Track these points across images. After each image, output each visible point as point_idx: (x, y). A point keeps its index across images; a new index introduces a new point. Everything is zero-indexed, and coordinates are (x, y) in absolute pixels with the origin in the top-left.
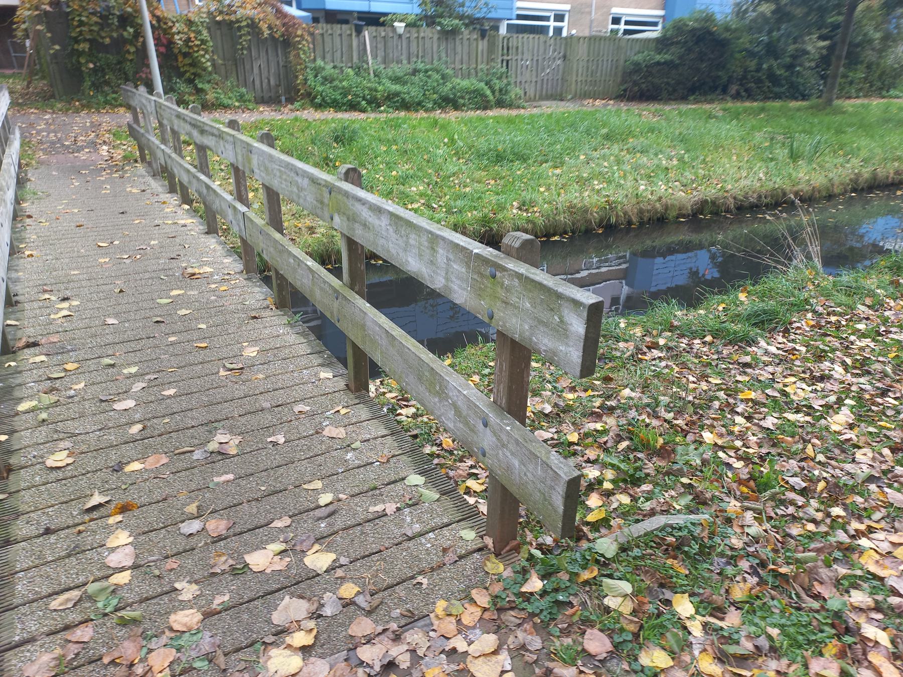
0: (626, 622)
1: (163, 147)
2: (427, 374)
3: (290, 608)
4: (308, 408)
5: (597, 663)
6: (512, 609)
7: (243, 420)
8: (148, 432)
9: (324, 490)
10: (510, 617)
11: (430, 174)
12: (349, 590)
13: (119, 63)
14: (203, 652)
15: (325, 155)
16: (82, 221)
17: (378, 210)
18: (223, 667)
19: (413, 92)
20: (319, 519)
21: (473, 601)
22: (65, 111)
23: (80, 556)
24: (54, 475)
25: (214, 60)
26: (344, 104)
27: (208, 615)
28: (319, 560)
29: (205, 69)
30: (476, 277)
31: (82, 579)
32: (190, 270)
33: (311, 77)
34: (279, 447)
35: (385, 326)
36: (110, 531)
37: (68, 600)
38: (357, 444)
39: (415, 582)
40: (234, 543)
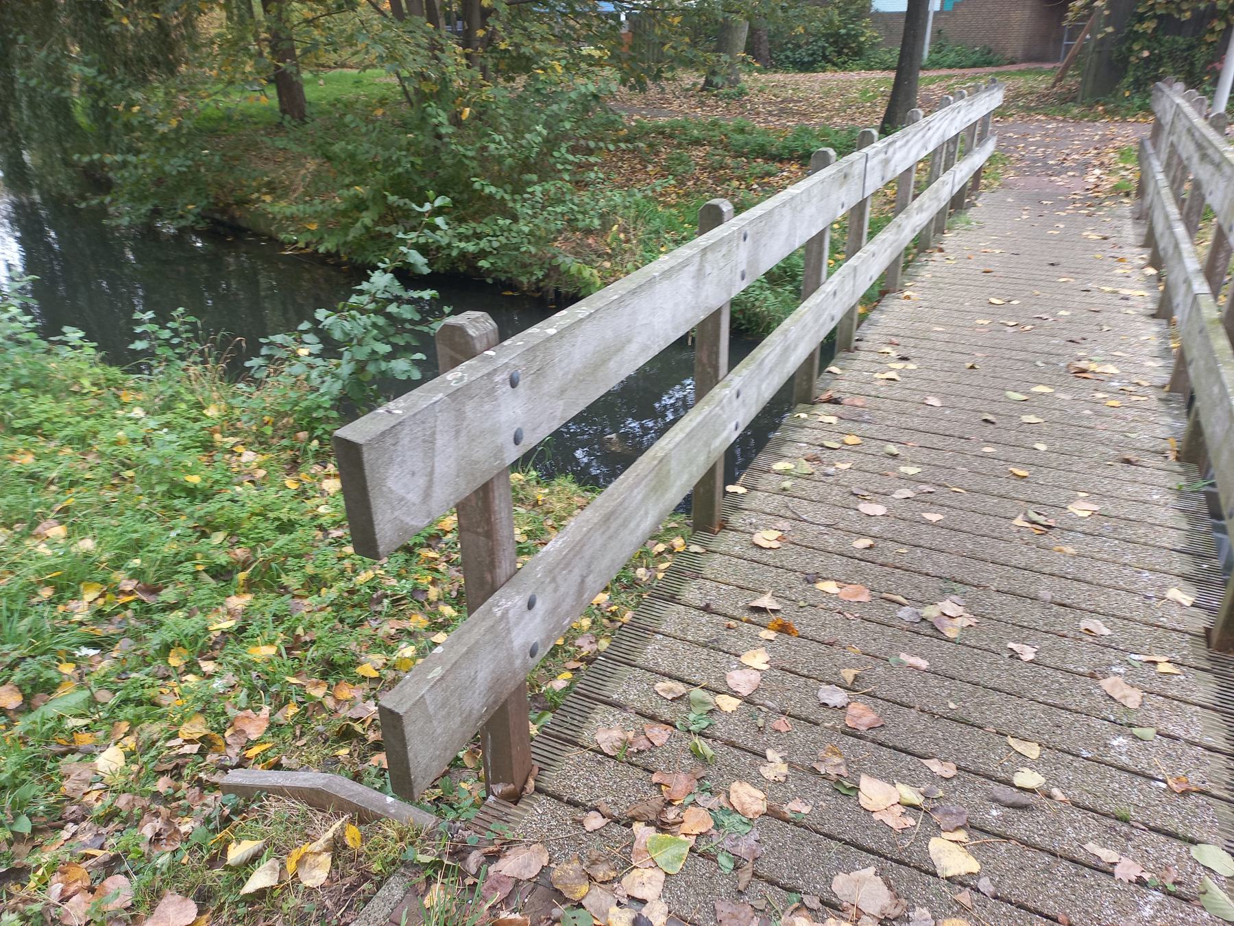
1: (1160, 176)
4: (1107, 632)
7: (998, 598)
9: (1035, 765)
13: (1191, 47)
14: (737, 851)
16: (994, 265)
18: (741, 887)
20: (995, 800)
22: (1077, 119)
24: (756, 554)
27: (772, 813)
28: (951, 856)
32: (1083, 364)
34: (1017, 664)
36: (755, 643)
37: (671, 690)
38: (1149, 733)
40: (865, 750)
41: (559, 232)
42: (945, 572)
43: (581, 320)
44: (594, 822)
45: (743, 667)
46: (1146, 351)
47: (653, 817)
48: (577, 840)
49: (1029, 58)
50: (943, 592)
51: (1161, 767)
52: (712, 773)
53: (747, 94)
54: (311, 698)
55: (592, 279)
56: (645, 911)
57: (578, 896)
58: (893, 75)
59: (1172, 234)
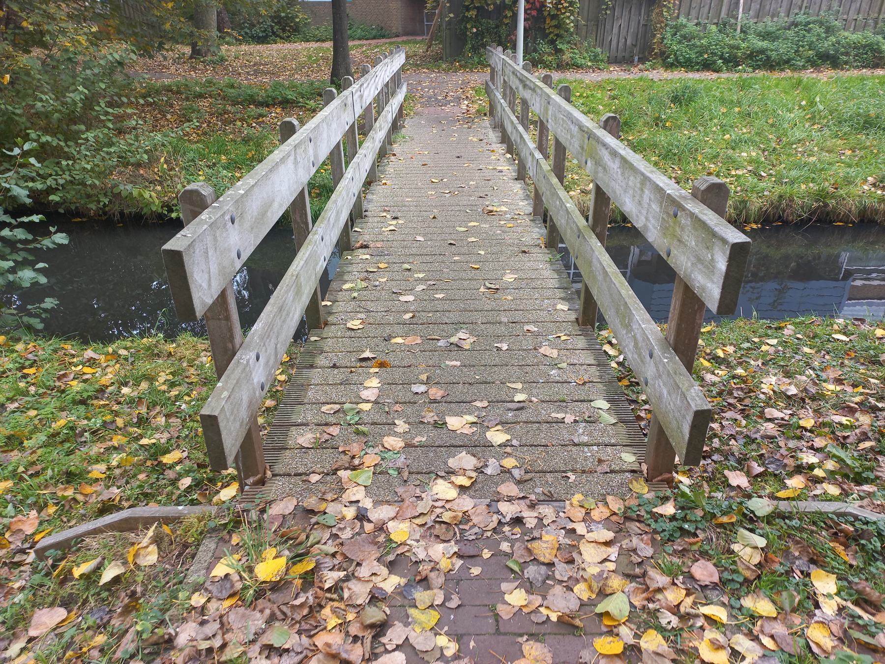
0: (743, 566)
1: (502, 101)
2: (622, 308)
3: (465, 460)
4: (536, 329)
5: (696, 586)
6: (639, 521)
7: (483, 327)
8: (415, 320)
9: (522, 391)
10: (634, 527)
11: (769, 140)
12: (509, 463)
13: (497, 27)
14: (397, 466)
15: (657, 115)
16: (426, 160)
17: (614, 154)
18: (405, 478)
19: (781, 48)
20: (509, 409)
21: (606, 504)
22: (446, 71)
23: (347, 386)
24: (349, 333)
25: (578, 21)
26: (697, 63)
27: (408, 445)
28: (497, 436)
29: (567, 30)
30: (664, 216)
31: (344, 400)
32: (490, 208)
33: (669, 35)
34: (501, 352)
35: (605, 264)
36: (369, 376)
37: (332, 409)
38: (564, 365)
39: (564, 475)
40: (443, 407)
41: (114, 167)
42: (455, 320)
43: (253, 186)
44: (314, 478)
45: (367, 388)
46: (518, 197)
47: (347, 465)
48: (309, 488)
49: (406, 34)
50: (456, 330)
51: (572, 377)
52: (371, 438)
53: (227, 60)
54: (64, 497)
55: (151, 200)
56: (360, 505)
57: (322, 509)
58: (329, 45)
59: (517, 130)
